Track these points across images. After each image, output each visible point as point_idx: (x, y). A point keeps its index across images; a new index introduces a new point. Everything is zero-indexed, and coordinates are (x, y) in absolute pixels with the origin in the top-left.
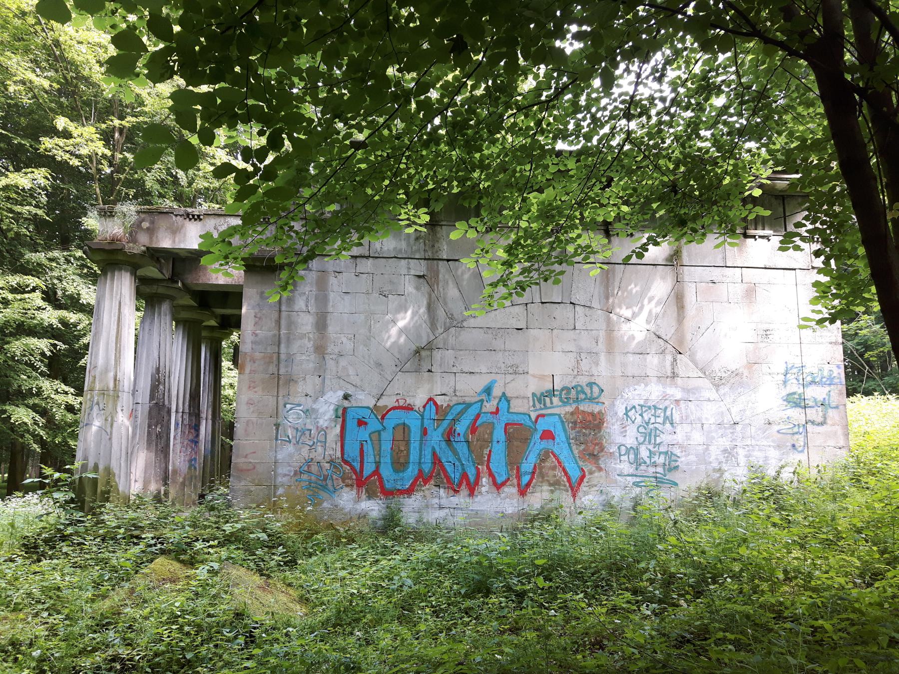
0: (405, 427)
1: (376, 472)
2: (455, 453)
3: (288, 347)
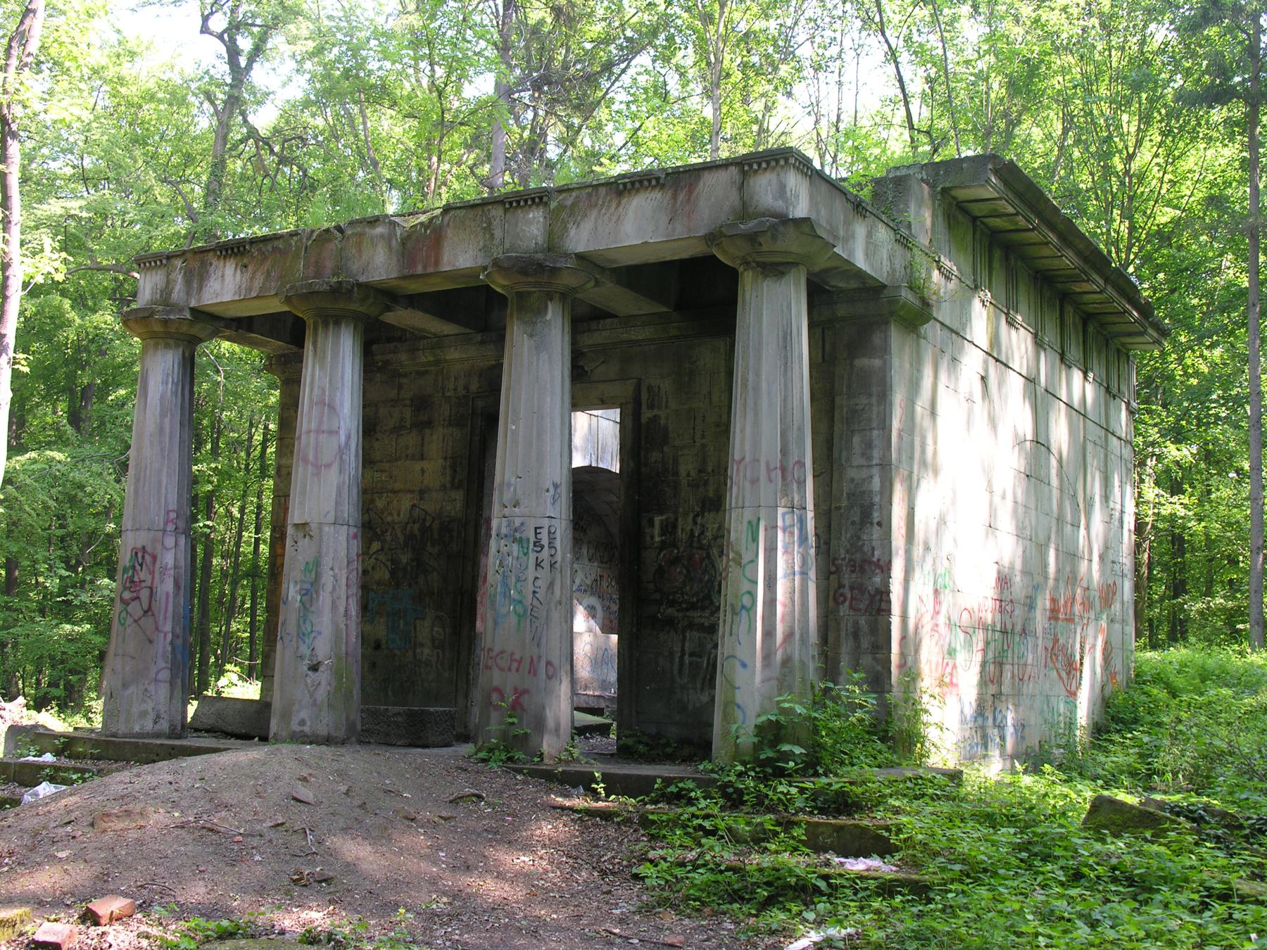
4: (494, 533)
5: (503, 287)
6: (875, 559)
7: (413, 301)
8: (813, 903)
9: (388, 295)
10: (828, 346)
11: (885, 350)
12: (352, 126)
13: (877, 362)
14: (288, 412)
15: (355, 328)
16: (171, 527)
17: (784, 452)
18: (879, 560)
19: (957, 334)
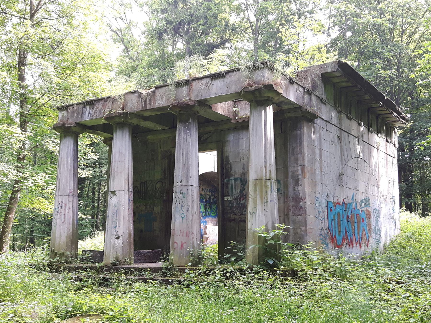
0: (339, 214)
1: (335, 236)
2: (348, 225)
4: (174, 191)
5: (176, 112)
6: (300, 197)
7: (146, 119)
8: (210, 206)
9: (138, 115)
10: (283, 128)
11: (301, 128)
12: (94, 193)
13: (299, 132)
14: (110, 152)
15: (129, 130)
16: (71, 194)
17: (266, 162)
18: (301, 197)
19: (329, 122)
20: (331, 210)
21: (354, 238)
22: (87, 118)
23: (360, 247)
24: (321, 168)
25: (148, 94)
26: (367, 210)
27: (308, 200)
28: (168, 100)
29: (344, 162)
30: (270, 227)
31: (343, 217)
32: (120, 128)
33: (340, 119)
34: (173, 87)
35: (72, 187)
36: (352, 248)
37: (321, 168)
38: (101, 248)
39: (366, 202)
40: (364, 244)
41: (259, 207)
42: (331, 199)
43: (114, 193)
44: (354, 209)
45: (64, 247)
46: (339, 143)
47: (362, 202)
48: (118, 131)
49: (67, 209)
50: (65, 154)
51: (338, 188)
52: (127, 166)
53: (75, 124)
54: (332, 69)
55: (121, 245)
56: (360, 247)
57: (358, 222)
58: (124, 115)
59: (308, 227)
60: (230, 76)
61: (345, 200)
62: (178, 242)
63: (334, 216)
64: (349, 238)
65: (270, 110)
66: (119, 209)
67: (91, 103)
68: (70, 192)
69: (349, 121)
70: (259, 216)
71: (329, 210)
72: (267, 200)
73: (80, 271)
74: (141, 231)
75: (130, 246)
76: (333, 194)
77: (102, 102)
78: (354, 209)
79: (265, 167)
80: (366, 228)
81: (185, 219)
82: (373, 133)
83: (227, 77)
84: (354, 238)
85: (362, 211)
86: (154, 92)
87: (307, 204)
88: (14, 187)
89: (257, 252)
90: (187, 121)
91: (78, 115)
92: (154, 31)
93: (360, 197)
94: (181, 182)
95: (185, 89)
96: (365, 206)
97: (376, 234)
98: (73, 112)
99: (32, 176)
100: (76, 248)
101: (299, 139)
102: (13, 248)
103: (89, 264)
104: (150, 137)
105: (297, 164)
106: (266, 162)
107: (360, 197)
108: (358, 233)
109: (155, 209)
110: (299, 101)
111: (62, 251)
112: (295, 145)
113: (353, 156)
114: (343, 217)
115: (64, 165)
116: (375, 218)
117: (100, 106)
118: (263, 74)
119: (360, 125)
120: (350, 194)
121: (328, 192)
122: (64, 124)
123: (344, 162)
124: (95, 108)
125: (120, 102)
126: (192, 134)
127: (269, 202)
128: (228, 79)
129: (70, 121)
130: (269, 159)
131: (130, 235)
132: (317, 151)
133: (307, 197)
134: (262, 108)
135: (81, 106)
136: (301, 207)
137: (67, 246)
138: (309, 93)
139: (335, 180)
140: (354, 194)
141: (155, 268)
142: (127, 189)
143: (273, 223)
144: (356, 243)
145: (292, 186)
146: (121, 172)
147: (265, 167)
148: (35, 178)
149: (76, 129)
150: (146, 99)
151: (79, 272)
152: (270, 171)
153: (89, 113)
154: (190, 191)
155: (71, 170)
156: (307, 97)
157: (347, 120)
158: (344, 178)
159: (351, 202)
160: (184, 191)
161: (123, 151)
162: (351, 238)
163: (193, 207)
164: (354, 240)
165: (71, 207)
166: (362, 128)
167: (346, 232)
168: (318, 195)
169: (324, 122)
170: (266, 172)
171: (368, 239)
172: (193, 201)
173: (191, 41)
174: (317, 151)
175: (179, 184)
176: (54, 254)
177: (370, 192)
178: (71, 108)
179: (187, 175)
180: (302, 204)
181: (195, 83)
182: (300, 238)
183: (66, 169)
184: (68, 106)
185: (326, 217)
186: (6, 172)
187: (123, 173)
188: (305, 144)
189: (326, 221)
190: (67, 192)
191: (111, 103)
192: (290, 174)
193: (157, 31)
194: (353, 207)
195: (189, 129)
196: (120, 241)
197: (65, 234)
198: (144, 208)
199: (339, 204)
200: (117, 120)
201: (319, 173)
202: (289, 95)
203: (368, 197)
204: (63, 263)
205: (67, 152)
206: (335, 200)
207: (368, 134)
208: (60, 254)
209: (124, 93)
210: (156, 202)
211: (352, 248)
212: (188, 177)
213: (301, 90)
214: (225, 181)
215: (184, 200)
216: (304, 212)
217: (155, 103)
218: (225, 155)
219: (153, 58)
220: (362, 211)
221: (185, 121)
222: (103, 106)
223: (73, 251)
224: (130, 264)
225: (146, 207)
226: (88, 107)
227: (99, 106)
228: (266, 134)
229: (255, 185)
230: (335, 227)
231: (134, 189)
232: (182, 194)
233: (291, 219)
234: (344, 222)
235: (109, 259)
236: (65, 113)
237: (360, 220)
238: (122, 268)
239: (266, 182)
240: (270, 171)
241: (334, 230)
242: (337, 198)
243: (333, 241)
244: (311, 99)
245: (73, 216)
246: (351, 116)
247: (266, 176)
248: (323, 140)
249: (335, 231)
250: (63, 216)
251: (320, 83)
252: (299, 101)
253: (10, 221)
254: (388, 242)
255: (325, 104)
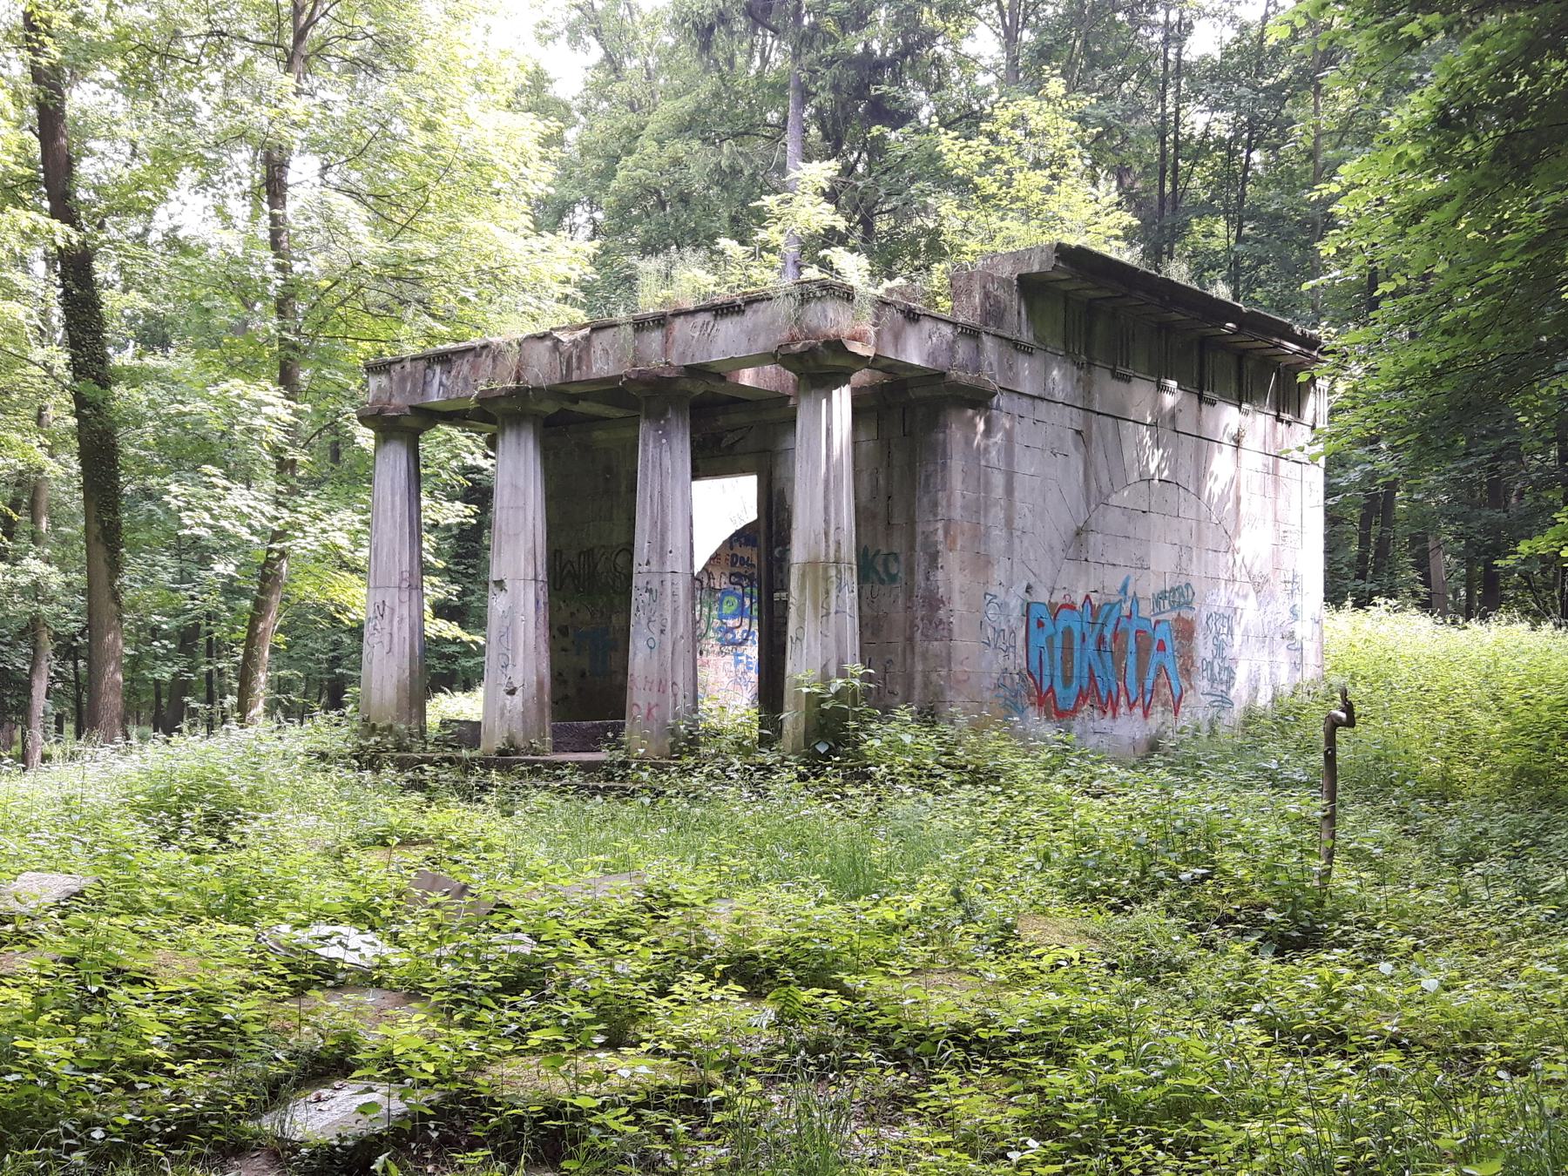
0: (1068, 633)
1: (1051, 688)
3: (986, 516)
13: (941, 436)
16: (405, 585)
17: (827, 522)
20: (1040, 624)
21: (1122, 693)
22: (435, 397)
23: (1146, 715)
24: (1009, 522)
25: (575, 343)
26: (1179, 619)
27: (958, 604)
28: (620, 360)
29: (1095, 495)
30: (833, 671)
31: (1083, 640)
32: (511, 425)
33: (1087, 386)
34: (629, 329)
35: (406, 567)
36: (1114, 717)
37: (1009, 522)
38: (475, 719)
39: (1180, 596)
40: (1160, 709)
41: (810, 626)
42: (1042, 596)
43: (500, 584)
44: (1129, 617)
45: (394, 713)
46: (1082, 449)
47: (1162, 596)
48: (507, 432)
49: (396, 619)
50: (388, 483)
51: (1069, 568)
52: (530, 518)
53: (408, 411)
54: (1041, 265)
55: (520, 708)
56: (1146, 715)
57: (1142, 653)
58: (520, 394)
59: (956, 668)
60: (755, 312)
61: (1093, 596)
62: (640, 703)
63: (1050, 639)
64: (1104, 694)
65: (842, 399)
66: (513, 621)
67: (445, 359)
68: (402, 580)
69: (1122, 385)
70: (809, 646)
71: (1033, 624)
72: (828, 610)
73: (425, 766)
74: (583, 675)
75: (541, 711)
76: (1049, 584)
77: (470, 357)
78: (1129, 617)
79: (826, 534)
80: (1172, 666)
81: (655, 651)
82: (1219, 404)
83: (749, 312)
84: (1122, 693)
85: (1158, 622)
86: (587, 339)
87: (957, 614)
88: (270, 550)
89: (802, 728)
90: (662, 415)
91: (414, 386)
92: (684, 21)
93: (1148, 586)
94: (648, 563)
95: (655, 337)
96: (1173, 608)
97: (1212, 680)
98: (403, 380)
99: (316, 518)
100: (422, 713)
101: (939, 454)
102: (269, 713)
103: (449, 752)
104: (599, 435)
105: (935, 515)
106: (827, 522)
107: (1148, 586)
108: (1141, 681)
109: (614, 618)
110: (935, 360)
111: (389, 721)
112: (931, 468)
113: (1135, 476)
114: (1083, 640)
115: (385, 511)
116: (1210, 638)
117: (466, 368)
118: (824, 311)
119: (1161, 388)
120: (1113, 580)
121: (1032, 580)
122: (381, 411)
123: (1095, 495)
124: (453, 373)
125: (512, 360)
126: (674, 446)
127: (832, 615)
128: (750, 318)
129: (396, 401)
130: (836, 514)
131: (540, 684)
132: (998, 480)
133: (956, 596)
134: (823, 393)
135: (421, 365)
136: (941, 621)
137: (399, 709)
138: (972, 333)
139: (1058, 546)
140: (1128, 578)
141: (589, 763)
142: (531, 575)
143: (841, 662)
144: (1131, 706)
145: (922, 567)
146: (516, 535)
147: (826, 534)
148: (322, 525)
149: (413, 423)
150: (570, 356)
151: (422, 771)
152: (838, 543)
153: (441, 384)
154: (668, 584)
155: (402, 524)
156: (963, 350)
157: (1115, 382)
158: (1094, 539)
159: (1115, 599)
160: (655, 585)
161: (521, 483)
162: (1110, 692)
163: (675, 623)
164: (1123, 699)
165: (406, 613)
166: (1169, 400)
167: (1092, 677)
168: (994, 590)
169: (1026, 402)
170: (828, 546)
171: (1177, 692)
172: (675, 610)
173: (804, 50)
174: (998, 480)
175: (645, 568)
176: (370, 728)
177: (1194, 570)
178: (398, 367)
179: (662, 548)
180: (942, 613)
181: (678, 323)
182: (935, 694)
183: (390, 521)
184: (391, 363)
185: (1020, 642)
186: (246, 510)
187: (522, 537)
188: (957, 464)
189: (1021, 652)
190: (396, 579)
191: (489, 361)
192: (919, 539)
193: (694, 23)
194: (1126, 612)
195: (666, 435)
196: (518, 698)
197: (395, 680)
198: (588, 617)
199: (1072, 607)
200: (504, 404)
201: (1004, 534)
202: (904, 350)
203: (1188, 585)
204: (388, 750)
205: (393, 479)
206: (1058, 598)
207: (1200, 410)
208: (383, 729)
209: (520, 336)
210: (616, 601)
211: (1114, 717)
212: (662, 553)
213: (947, 330)
214: (776, 552)
215: (654, 606)
216: (945, 633)
217: (589, 367)
218: (776, 487)
219: (687, 103)
220: (1158, 622)
221: (657, 416)
222: (474, 368)
223: (415, 722)
224: (544, 753)
225: (592, 615)
226: (438, 369)
227: (464, 366)
228: (828, 456)
229: (803, 576)
230: (1052, 666)
231: (548, 575)
232: (650, 591)
233: (918, 649)
234: (1085, 654)
235: (493, 742)
236: (383, 380)
237: (1151, 645)
238: (520, 761)
239: (826, 570)
240: (838, 543)
241: (1046, 671)
242: (1063, 593)
243: (1046, 702)
244: (979, 350)
245: (412, 639)
246: (1129, 372)
247: (827, 554)
248: (1017, 448)
249: (1052, 677)
250: (386, 639)
251: (1014, 303)
252: (935, 360)
253: (263, 639)
254: (1264, 699)
255: (1031, 354)
